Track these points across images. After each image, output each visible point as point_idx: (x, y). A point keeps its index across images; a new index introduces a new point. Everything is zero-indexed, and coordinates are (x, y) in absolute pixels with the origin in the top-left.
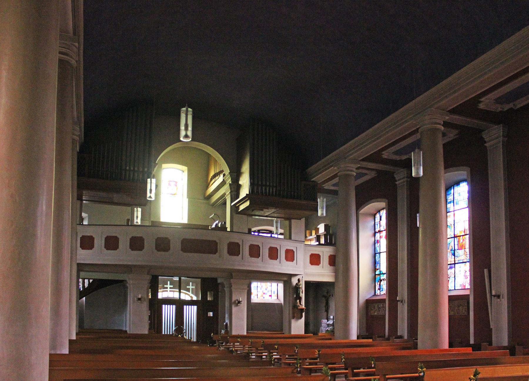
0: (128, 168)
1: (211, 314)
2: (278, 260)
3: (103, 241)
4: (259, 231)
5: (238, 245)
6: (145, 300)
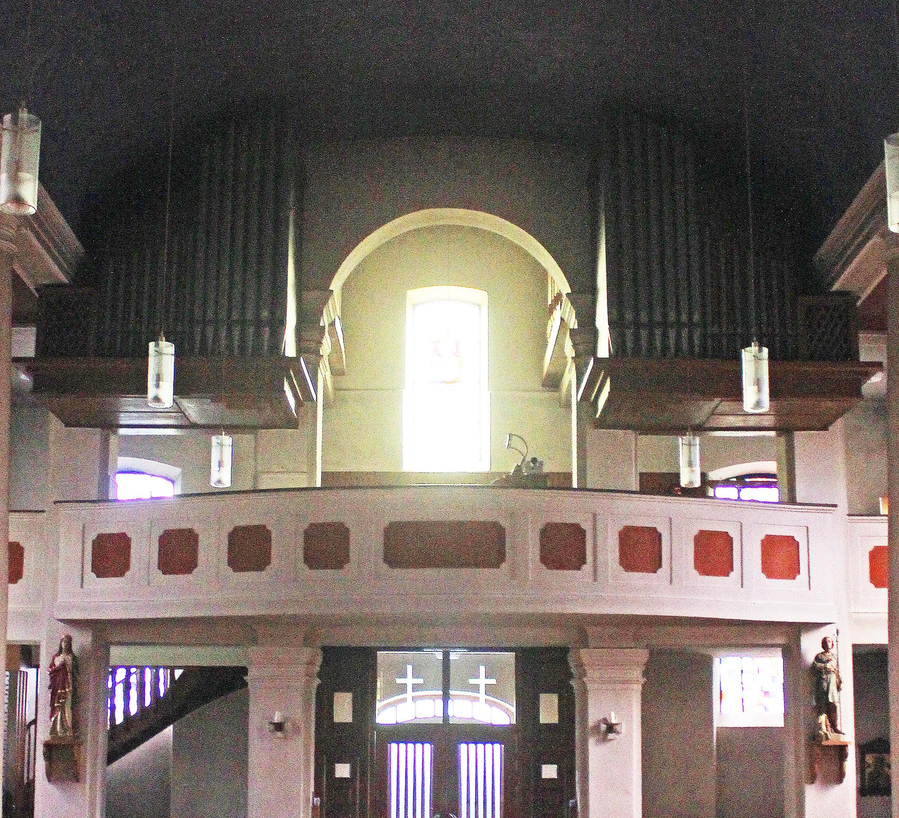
0: (265, 314)
1: (549, 771)
2: (735, 575)
3: (155, 547)
4: (741, 481)
5: (578, 532)
6: (297, 730)
